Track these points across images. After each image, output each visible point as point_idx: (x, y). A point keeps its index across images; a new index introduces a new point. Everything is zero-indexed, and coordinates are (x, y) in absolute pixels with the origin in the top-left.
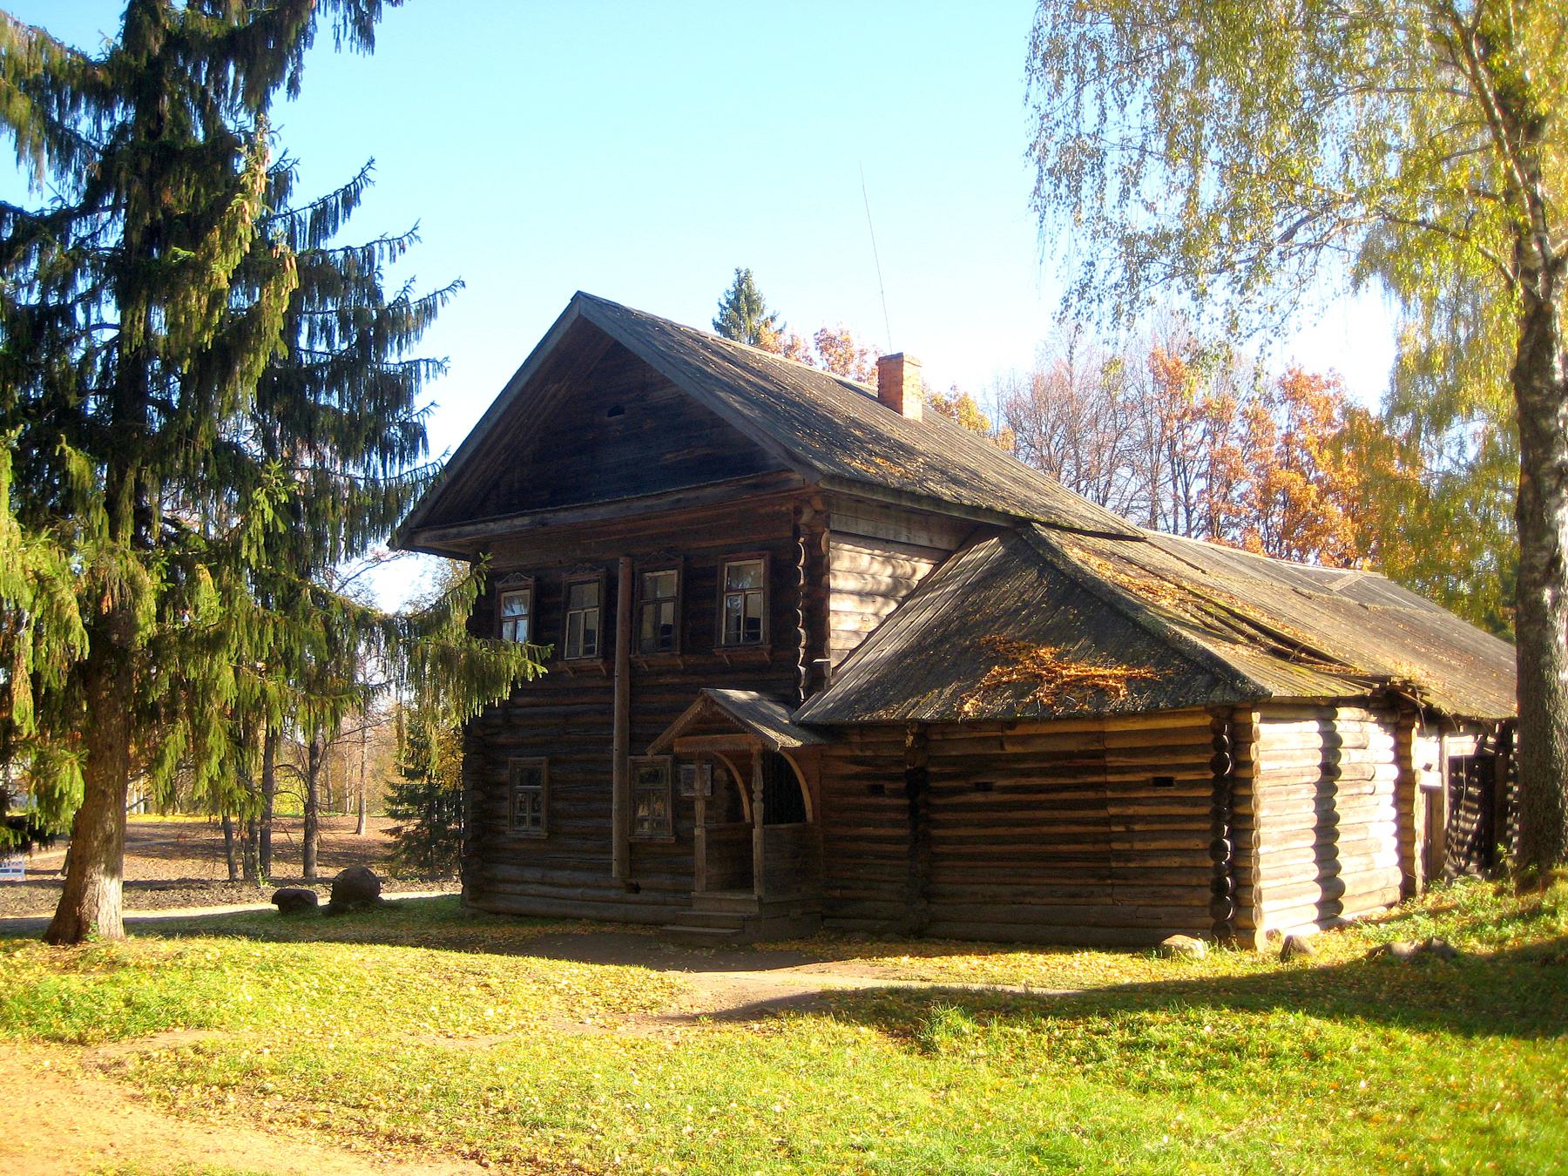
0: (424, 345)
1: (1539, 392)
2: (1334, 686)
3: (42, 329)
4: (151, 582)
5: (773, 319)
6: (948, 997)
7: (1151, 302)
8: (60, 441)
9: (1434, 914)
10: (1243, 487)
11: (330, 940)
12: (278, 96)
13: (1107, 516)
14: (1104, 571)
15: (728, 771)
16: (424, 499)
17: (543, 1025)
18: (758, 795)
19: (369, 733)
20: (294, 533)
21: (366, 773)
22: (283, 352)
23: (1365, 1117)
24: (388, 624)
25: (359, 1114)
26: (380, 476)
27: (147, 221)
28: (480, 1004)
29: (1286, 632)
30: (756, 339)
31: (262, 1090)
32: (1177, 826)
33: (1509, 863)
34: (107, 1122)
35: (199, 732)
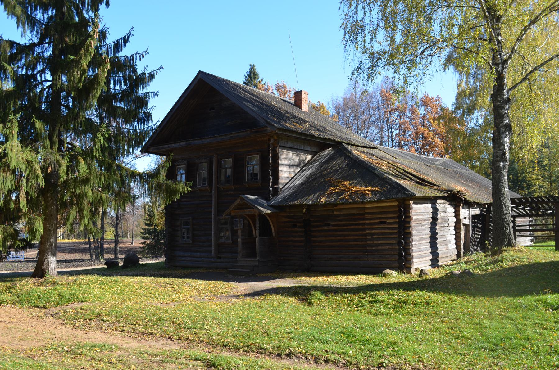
0: (151, 87)
1: (499, 101)
2: (436, 193)
3: (25, 83)
4: (64, 163)
5: (262, 80)
6: (316, 288)
7: (379, 73)
8: (33, 117)
9: (466, 263)
10: (410, 133)
11: (123, 276)
12: (102, 7)
13: (367, 141)
14: (364, 158)
15: (248, 221)
16: (152, 136)
17: (191, 299)
18: (257, 228)
19: (135, 212)
20: (110, 147)
21: (134, 225)
22: (106, 89)
23: (443, 321)
24: (141, 175)
25: (133, 327)
26: (137, 129)
27: (60, 47)
28: (171, 293)
29: (421, 177)
30: (257, 87)
31: (103, 320)
32: (387, 236)
33: (489, 247)
34: (54, 331)
35: (81, 210)
